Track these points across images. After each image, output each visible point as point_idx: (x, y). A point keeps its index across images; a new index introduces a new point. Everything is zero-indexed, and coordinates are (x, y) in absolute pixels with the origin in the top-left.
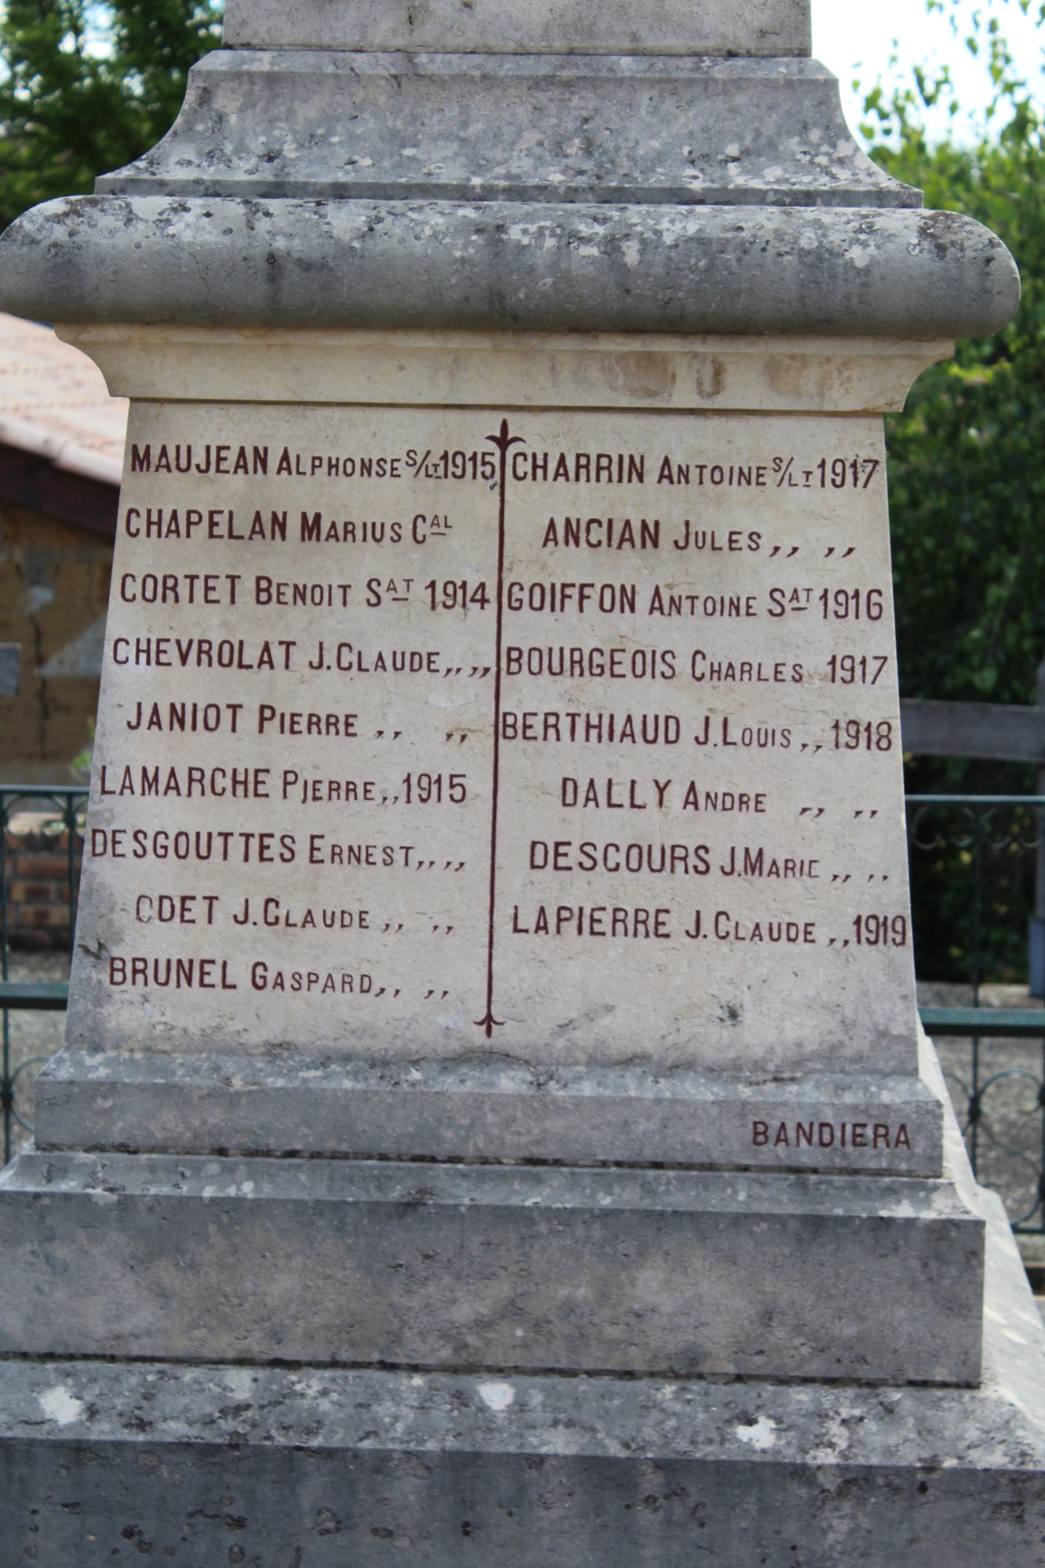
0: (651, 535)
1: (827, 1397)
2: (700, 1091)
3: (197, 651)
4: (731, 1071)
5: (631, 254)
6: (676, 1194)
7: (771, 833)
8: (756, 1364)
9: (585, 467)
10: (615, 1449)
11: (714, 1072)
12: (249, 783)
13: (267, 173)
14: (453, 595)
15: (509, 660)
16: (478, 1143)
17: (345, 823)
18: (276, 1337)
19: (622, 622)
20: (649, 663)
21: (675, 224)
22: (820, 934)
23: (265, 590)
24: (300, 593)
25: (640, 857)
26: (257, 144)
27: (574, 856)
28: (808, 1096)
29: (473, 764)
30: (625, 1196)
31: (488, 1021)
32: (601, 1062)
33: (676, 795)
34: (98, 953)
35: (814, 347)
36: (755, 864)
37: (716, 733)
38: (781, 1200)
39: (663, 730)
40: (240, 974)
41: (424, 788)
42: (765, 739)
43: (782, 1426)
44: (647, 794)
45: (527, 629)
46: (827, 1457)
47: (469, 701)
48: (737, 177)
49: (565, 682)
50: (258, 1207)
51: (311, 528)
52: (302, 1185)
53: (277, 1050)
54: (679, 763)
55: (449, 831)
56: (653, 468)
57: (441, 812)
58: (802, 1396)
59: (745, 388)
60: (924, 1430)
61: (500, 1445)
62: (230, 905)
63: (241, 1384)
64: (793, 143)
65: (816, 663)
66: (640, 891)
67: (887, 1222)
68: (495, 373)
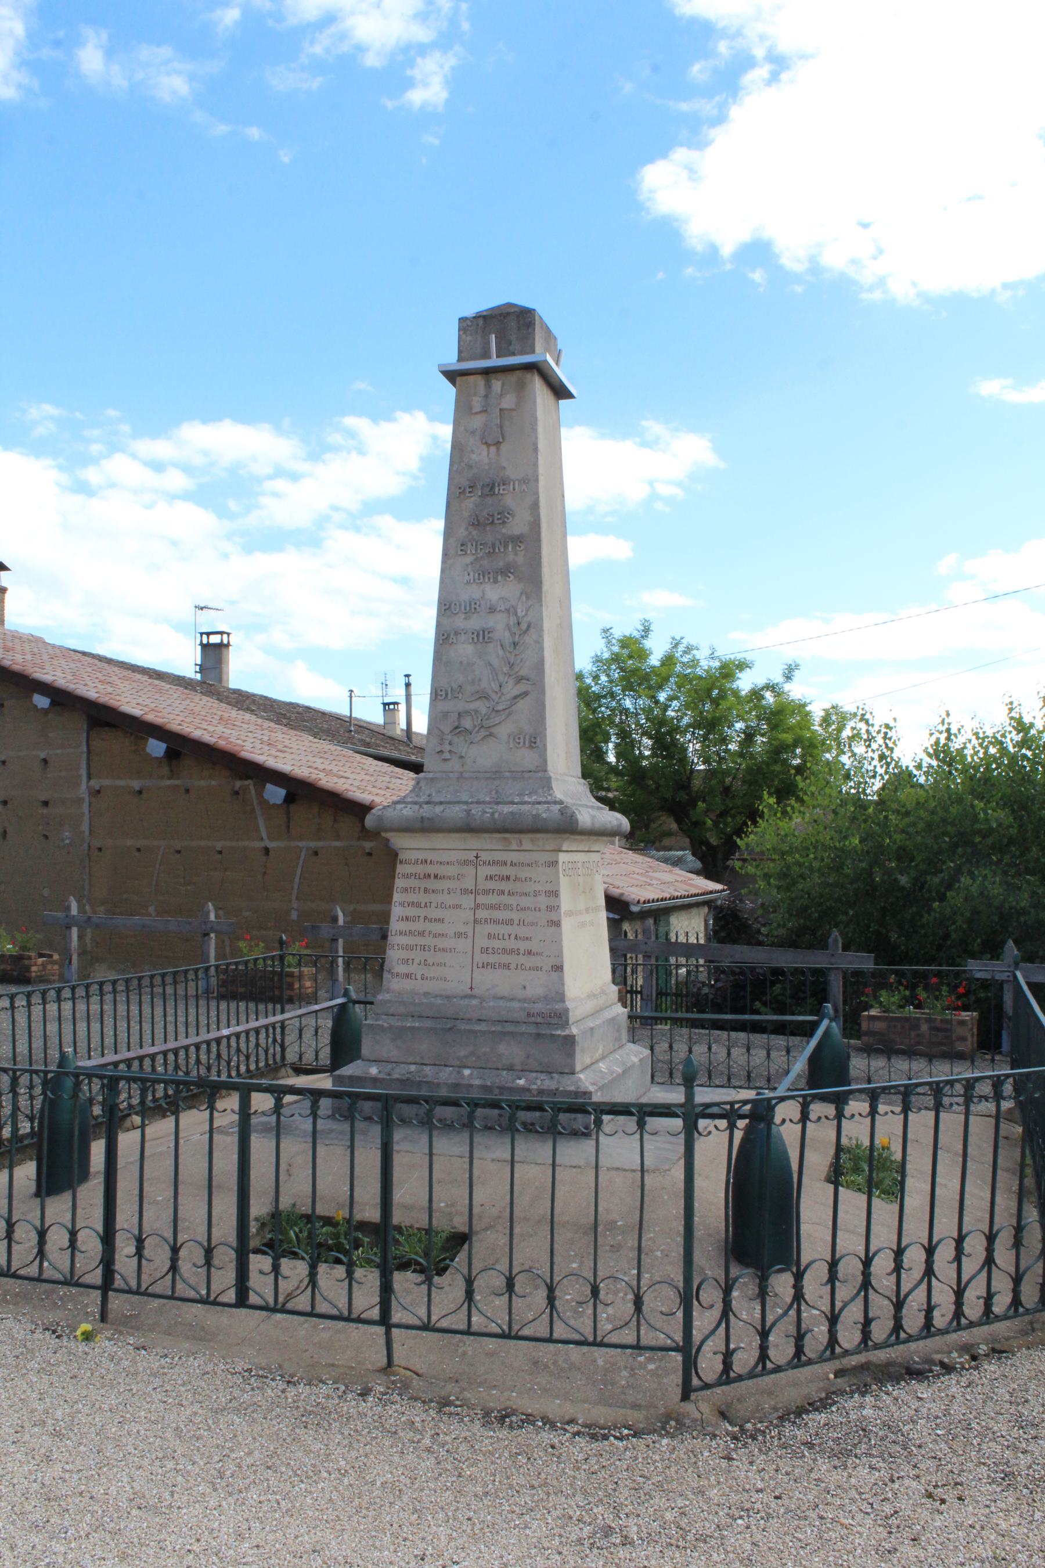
0: (508, 878)
1: (539, 1075)
2: (516, 1005)
3: (412, 904)
4: (524, 1000)
5: (496, 815)
6: (509, 1028)
7: (533, 946)
8: (526, 1067)
9: (495, 863)
10: (489, 1084)
11: (519, 1001)
12: (421, 934)
13: (427, 799)
14: (466, 892)
15: (477, 906)
16: (468, 1016)
17: (442, 943)
18: (422, 1058)
19: (502, 897)
20: (507, 907)
21: (507, 809)
22: (544, 969)
23: (426, 890)
24: (433, 891)
25: (505, 951)
26: (427, 793)
27: (490, 950)
28: (540, 1007)
29: (469, 929)
30: (499, 1028)
31: (471, 988)
32: (496, 998)
33: (513, 937)
34: (389, 971)
35: (539, 835)
36: (530, 953)
37: (522, 923)
38: (532, 1030)
39: (510, 922)
40: (419, 977)
41: (459, 935)
42: (532, 924)
43: (527, 1080)
44: (506, 937)
45: (482, 899)
46: (535, 1087)
47: (469, 915)
48: (526, 799)
49: (489, 911)
50: (419, 1028)
51: (436, 877)
52: (429, 1024)
53: (426, 994)
54: (514, 930)
55: (464, 945)
56: (509, 863)
57: (462, 940)
58: (534, 1075)
59: (527, 844)
60: (558, 1082)
61: (465, 1082)
62: (417, 961)
63: (413, 1068)
64: (540, 791)
65: (543, 907)
66: (505, 959)
67: (553, 1035)
68: (474, 842)
